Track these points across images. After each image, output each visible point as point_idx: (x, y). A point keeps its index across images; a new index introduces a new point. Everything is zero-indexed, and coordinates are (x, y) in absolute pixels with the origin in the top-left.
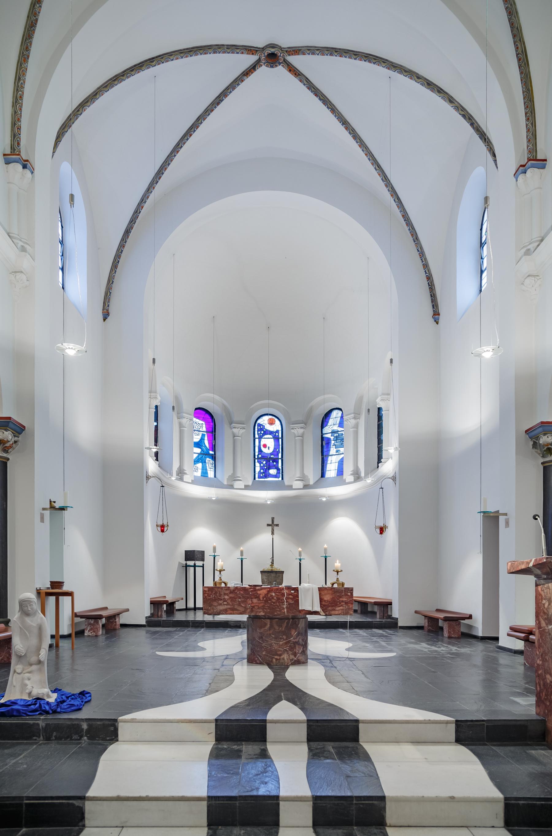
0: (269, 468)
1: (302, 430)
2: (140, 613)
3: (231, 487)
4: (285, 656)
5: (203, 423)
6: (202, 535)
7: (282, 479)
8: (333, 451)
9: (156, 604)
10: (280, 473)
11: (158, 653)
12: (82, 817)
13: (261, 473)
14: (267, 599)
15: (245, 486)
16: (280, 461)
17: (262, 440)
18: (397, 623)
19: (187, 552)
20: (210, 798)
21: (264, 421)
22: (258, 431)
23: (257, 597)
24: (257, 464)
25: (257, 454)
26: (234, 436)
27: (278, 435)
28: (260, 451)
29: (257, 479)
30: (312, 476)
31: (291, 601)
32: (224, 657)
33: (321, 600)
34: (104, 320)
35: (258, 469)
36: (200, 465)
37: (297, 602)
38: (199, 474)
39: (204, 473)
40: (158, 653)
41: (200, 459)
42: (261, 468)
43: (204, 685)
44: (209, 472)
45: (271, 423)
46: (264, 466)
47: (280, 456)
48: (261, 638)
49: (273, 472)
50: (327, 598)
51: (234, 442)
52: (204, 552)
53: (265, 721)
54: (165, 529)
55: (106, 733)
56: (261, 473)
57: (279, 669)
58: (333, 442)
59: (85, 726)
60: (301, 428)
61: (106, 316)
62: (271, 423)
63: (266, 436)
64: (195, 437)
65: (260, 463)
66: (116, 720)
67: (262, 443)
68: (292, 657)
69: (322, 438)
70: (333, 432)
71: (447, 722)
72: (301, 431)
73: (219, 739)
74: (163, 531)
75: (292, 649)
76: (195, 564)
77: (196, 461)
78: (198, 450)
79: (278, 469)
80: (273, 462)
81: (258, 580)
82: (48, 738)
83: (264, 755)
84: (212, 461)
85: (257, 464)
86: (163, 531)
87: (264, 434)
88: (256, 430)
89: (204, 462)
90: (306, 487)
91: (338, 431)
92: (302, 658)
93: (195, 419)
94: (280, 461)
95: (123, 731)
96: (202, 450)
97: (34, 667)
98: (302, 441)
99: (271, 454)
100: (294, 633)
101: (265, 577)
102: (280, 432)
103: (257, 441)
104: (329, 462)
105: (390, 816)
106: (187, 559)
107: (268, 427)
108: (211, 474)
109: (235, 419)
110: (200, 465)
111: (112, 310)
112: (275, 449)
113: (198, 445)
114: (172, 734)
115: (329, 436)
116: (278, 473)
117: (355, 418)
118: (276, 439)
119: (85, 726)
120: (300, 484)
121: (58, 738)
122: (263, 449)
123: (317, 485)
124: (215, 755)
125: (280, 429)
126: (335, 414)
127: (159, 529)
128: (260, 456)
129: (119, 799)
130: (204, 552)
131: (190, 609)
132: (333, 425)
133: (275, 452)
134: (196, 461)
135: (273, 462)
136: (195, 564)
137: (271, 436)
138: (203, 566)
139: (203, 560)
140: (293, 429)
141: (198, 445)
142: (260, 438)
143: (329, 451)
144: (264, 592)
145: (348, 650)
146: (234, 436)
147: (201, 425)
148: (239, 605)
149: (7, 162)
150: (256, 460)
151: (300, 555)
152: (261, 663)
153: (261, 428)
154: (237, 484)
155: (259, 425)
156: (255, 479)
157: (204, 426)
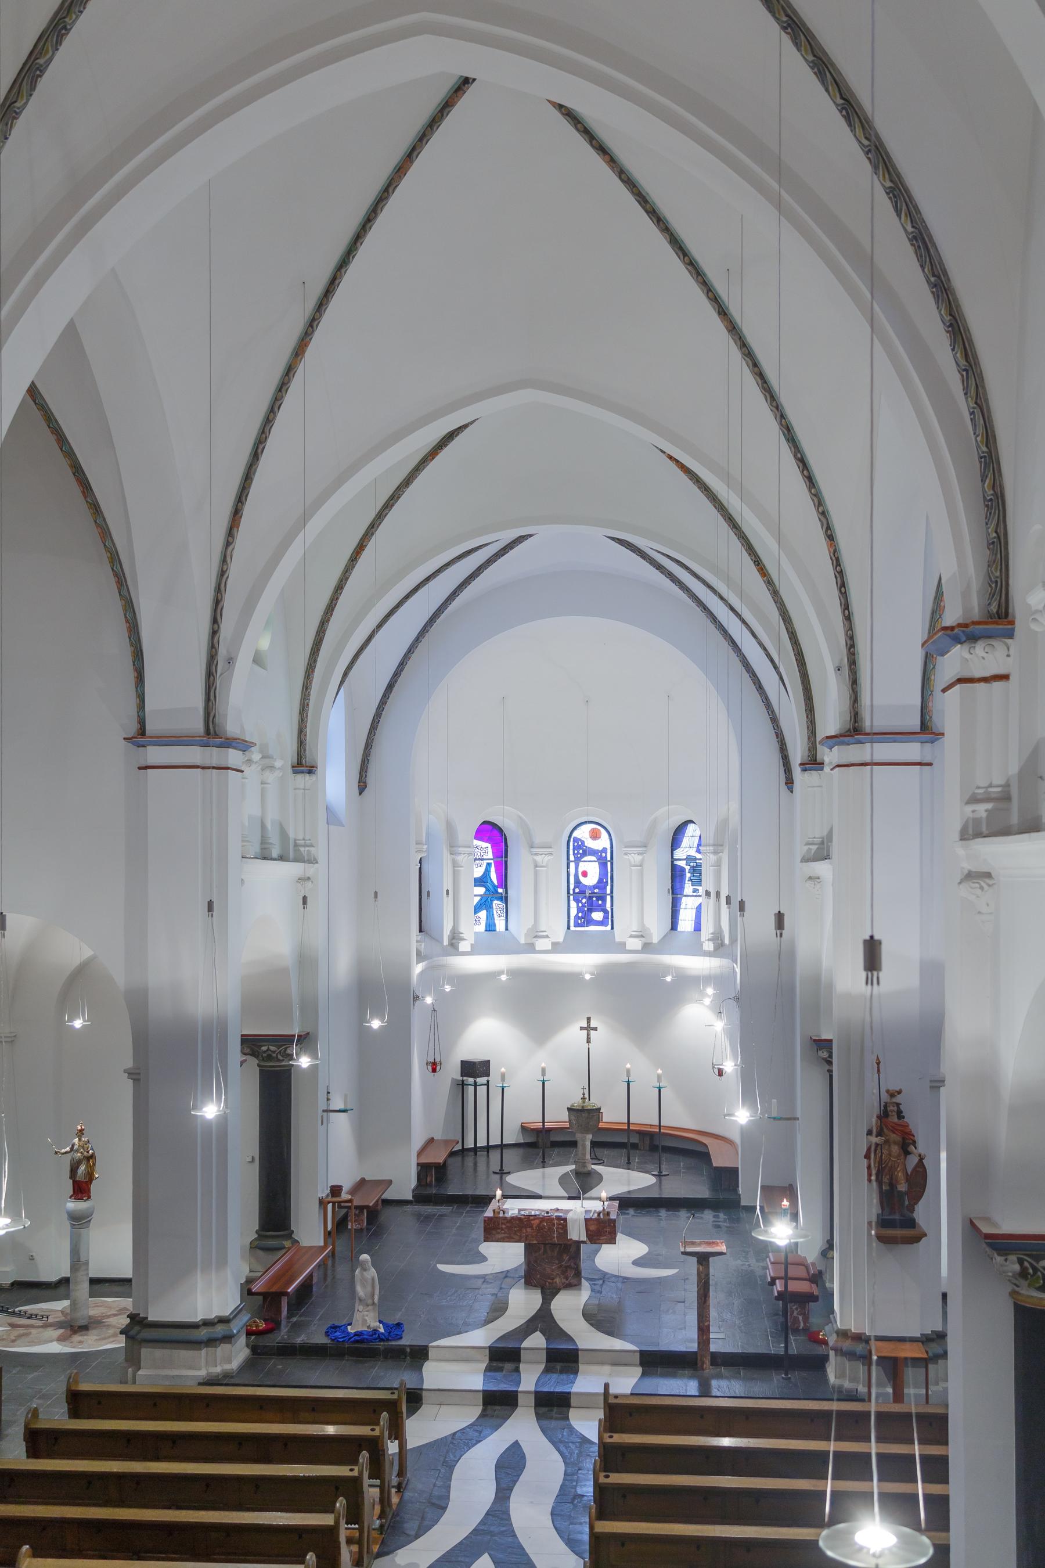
0: (590, 911)
1: (640, 857)
2: (404, 1183)
3: (530, 948)
4: (557, 1280)
5: (489, 845)
6: (487, 1034)
7: (612, 928)
8: (688, 888)
9: (424, 1169)
10: (609, 918)
11: (442, 1267)
12: (421, 1399)
13: (579, 918)
14: (540, 1228)
15: (554, 944)
16: (608, 898)
17: (581, 864)
18: (739, 1202)
19: (464, 1064)
20: (484, 1391)
21: (583, 833)
22: (574, 849)
23: (531, 1227)
24: (573, 904)
25: (572, 887)
26: (536, 866)
27: (606, 857)
28: (578, 882)
29: (572, 928)
30: (657, 928)
31: (560, 1231)
32: (504, 1275)
33: (587, 1230)
34: (360, 794)
35: (574, 911)
36: (483, 914)
37: (566, 1231)
38: (481, 928)
39: (490, 927)
40: (442, 1267)
41: (484, 904)
42: (579, 910)
43: (483, 1314)
44: (497, 922)
45: (595, 835)
46: (583, 906)
47: (608, 891)
48: (536, 1262)
49: (597, 916)
50: (593, 1228)
51: (536, 874)
52: (489, 1061)
53: (520, 1348)
54: (438, 1068)
55: (419, 1355)
56: (579, 918)
57: (549, 1295)
58: (688, 875)
59: (408, 1350)
60: (639, 854)
61: (362, 787)
62: (595, 835)
63: (585, 858)
64: (475, 870)
65: (577, 901)
66: (427, 1346)
67: (580, 870)
68: (564, 1280)
69: (674, 867)
70: (689, 859)
71: (635, 1351)
72: (638, 858)
73: (491, 1359)
74: (434, 1070)
75: (564, 1272)
76: (475, 1082)
77: (477, 909)
78: (481, 890)
79: (605, 912)
80: (598, 899)
81: (565, 1116)
82: (386, 1358)
83: (517, 1370)
84: (502, 904)
85: (573, 904)
86: (434, 1070)
87: (584, 854)
88: (571, 847)
89: (489, 908)
90: (647, 948)
91: (696, 859)
92: (574, 1281)
93: (476, 842)
94: (608, 898)
95: (431, 1353)
96: (487, 889)
97: (370, 1307)
98: (641, 874)
99: (595, 887)
100: (566, 1258)
101: (573, 1118)
102: (609, 851)
103: (572, 865)
104: (683, 906)
105: (574, 1401)
106: (464, 1073)
107: (590, 844)
108: (500, 925)
109: (537, 840)
110: (483, 914)
111: (371, 780)
112: (600, 881)
113: (480, 882)
114: (462, 1355)
115: (682, 864)
116: (606, 917)
117: (715, 853)
118: (603, 864)
119: (408, 1350)
120: (635, 944)
121: (392, 1357)
122: (582, 879)
123: (664, 946)
124: (488, 1369)
125: (608, 846)
126: (691, 828)
127: (430, 1068)
128: (577, 890)
129: (439, 1390)
130: (489, 1061)
131: (469, 1150)
132: (687, 848)
133: (601, 884)
134: (477, 909)
135: (598, 899)
136: (475, 1082)
137: (594, 858)
138: (488, 1084)
139: (488, 1075)
140: (626, 854)
141: (480, 882)
142: (578, 860)
143: (682, 888)
144: (537, 1221)
145: (637, 1263)
146: (536, 866)
147: (486, 850)
148: (515, 1234)
149: (295, 772)
150: (572, 897)
151: (628, 1075)
152: (535, 1286)
153: (580, 845)
154: (542, 944)
155: (576, 840)
156: (569, 928)
157: (490, 850)
